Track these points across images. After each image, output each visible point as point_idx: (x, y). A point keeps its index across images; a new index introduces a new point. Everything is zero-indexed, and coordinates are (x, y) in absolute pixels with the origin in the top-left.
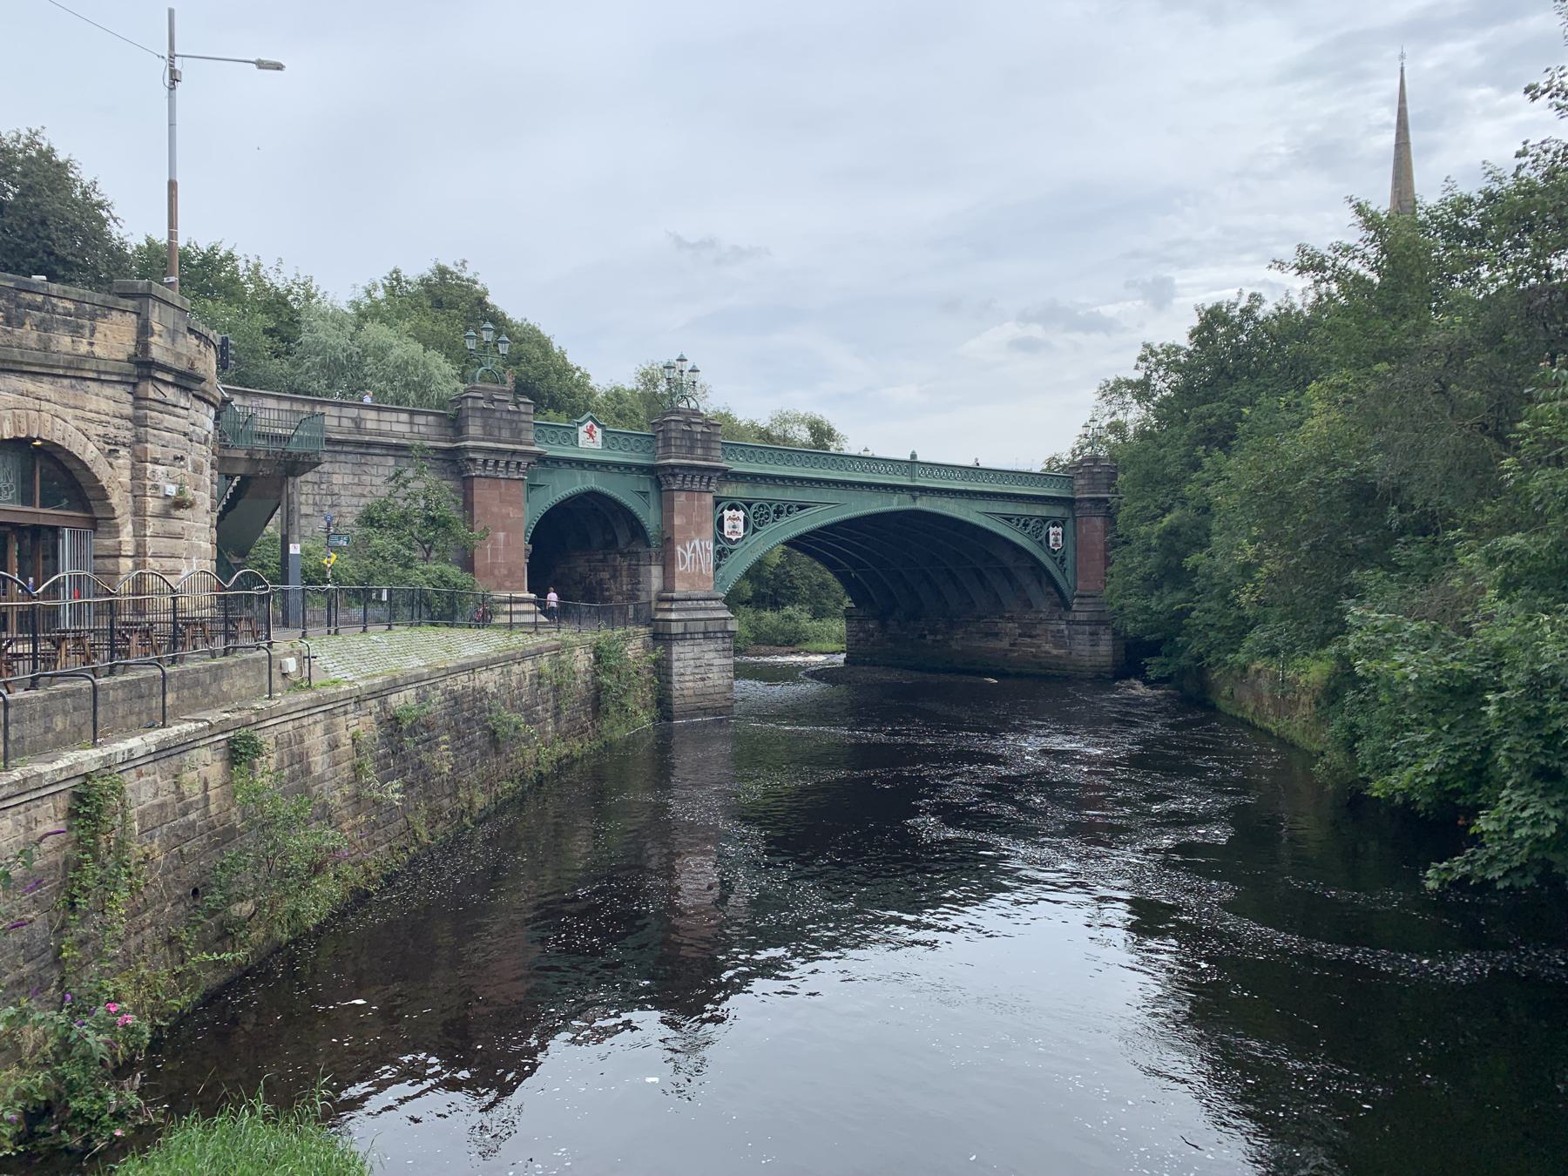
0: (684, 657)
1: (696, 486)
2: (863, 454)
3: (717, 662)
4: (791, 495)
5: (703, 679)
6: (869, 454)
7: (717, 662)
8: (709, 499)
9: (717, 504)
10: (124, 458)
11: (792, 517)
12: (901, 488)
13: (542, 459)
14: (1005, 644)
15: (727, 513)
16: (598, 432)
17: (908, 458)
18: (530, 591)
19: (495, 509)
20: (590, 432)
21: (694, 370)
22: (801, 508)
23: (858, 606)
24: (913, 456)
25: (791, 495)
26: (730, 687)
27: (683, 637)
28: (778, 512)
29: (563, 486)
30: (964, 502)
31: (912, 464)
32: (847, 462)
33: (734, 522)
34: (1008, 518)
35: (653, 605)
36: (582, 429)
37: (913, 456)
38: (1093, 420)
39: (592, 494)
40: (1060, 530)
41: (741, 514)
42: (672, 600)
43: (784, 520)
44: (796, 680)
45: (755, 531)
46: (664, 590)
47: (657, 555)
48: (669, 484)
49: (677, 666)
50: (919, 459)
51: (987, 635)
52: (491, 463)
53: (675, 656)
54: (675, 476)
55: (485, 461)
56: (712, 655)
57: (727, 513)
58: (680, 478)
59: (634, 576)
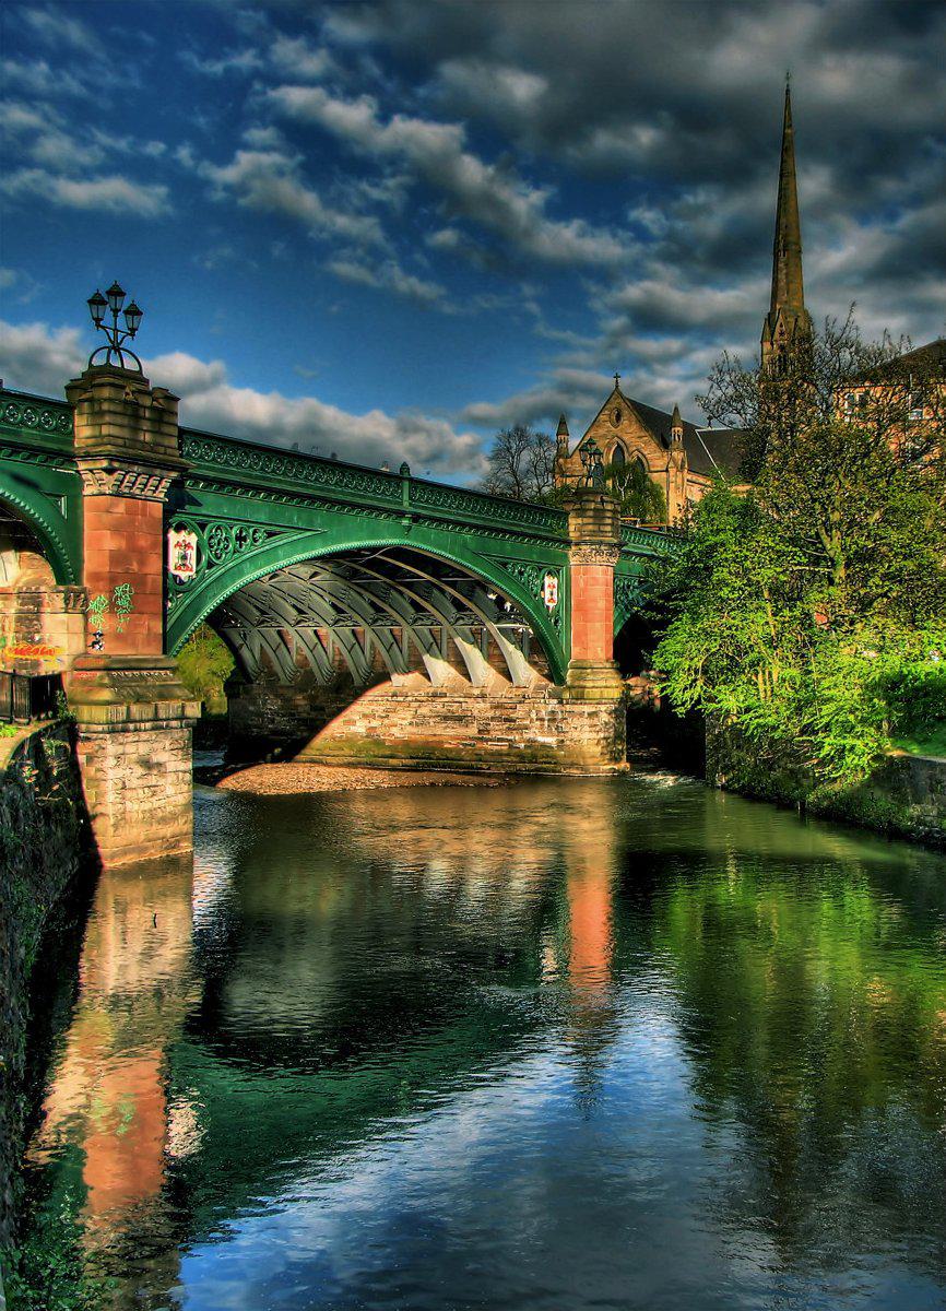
17: (329, 456)
24: (334, 455)
37: (334, 455)
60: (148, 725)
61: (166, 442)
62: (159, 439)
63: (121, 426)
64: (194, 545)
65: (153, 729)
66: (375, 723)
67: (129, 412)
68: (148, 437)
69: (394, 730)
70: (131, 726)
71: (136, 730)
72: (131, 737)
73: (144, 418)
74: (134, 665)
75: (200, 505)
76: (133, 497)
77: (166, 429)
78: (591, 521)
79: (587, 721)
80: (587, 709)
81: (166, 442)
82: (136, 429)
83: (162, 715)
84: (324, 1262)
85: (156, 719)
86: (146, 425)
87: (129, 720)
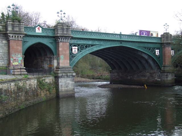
0: (62, 82)
1: (65, 41)
2: (114, 33)
3: (70, 83)
4: (90, 42)
5: (67, 87)
6: (115, 33)
7: (70, 83)
8: (68, 44)
9: (71, 45)
10: (27, 39)
11: (90, 48)
12: (118, 41)
13: (27, 36)
14: (146, 78)
15: (73, 47)
16: (41, 29)
17: (119, 33)
18: (24, 67)
19: (15, 47)
20: (39, 29)
21: (64, 14)
22: (92, 46)
23: (113, 70)
24: (121, 33)
25: (90, 42)
26: (74, 89)
27: (62, 77)
28: (86, 47)
29: (32, 42)
30: (151, 44)
31: (120, 35)
32: (88, 33)
33: (75, 50)
34: (139, 47)
35: (55, 70)
36: (37, 28)
37: (121, 33)
38: (166, 24)
39: (39, 44)
40: (158, 50)
41: (77, 47)
42: (59, 68)
43: (87, 49)
44: (96, 88)
45: (80, 51)
46: (57, 66)
47: (56, 57)
48: (58, 41)
49: (60, 84)
50: (122, 34)
51: (142, 76)
52: (16, 36)
53: (59, 82)
54: (59, 38)
55: (12, 36)
56: (69, 81)
57: (73, 47)
58: (61, 39)
59: (50, 61)
60: (66, 77)
61: (69, 33)
62: (67, 33)
63: (61, 31)
64: (77, 49)
65: (67, 77)
66: (131, 77)
67: (62, 29)
68: (65, 33)
69: (134, 78)
70: (63, 77)
71: (64, 77)
72: (63, 78)
73: (65, 30)
74: (64, 67)
75: (49, 42)
76: (63, 42)
77: (68, 31)
78: (165, 39)
79: (165, 76)
80: (165, 74)
81: (69, 33)
82: (63, 32)
83: (68, 75)
84: (26, 134)
85: (67, 76)
86: (65, 31)
87: (62, 76)
